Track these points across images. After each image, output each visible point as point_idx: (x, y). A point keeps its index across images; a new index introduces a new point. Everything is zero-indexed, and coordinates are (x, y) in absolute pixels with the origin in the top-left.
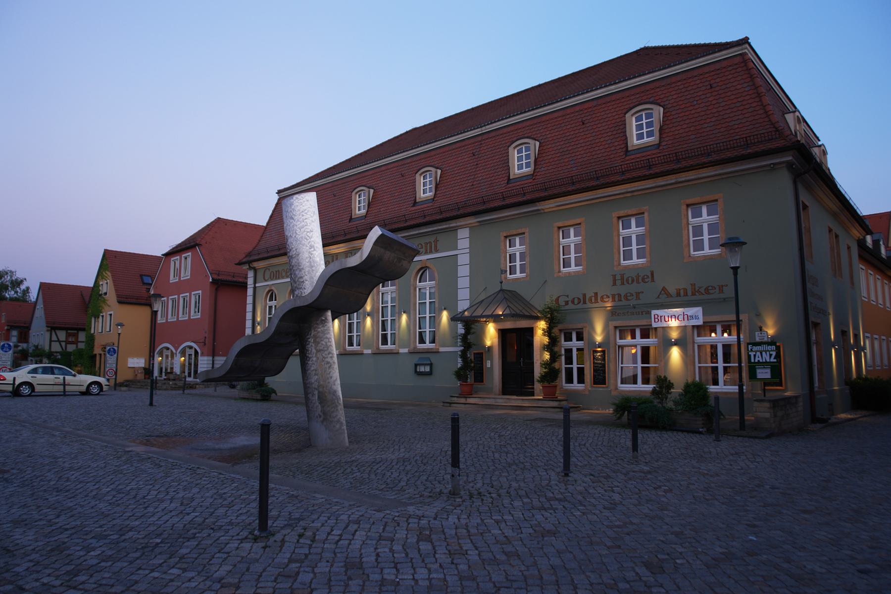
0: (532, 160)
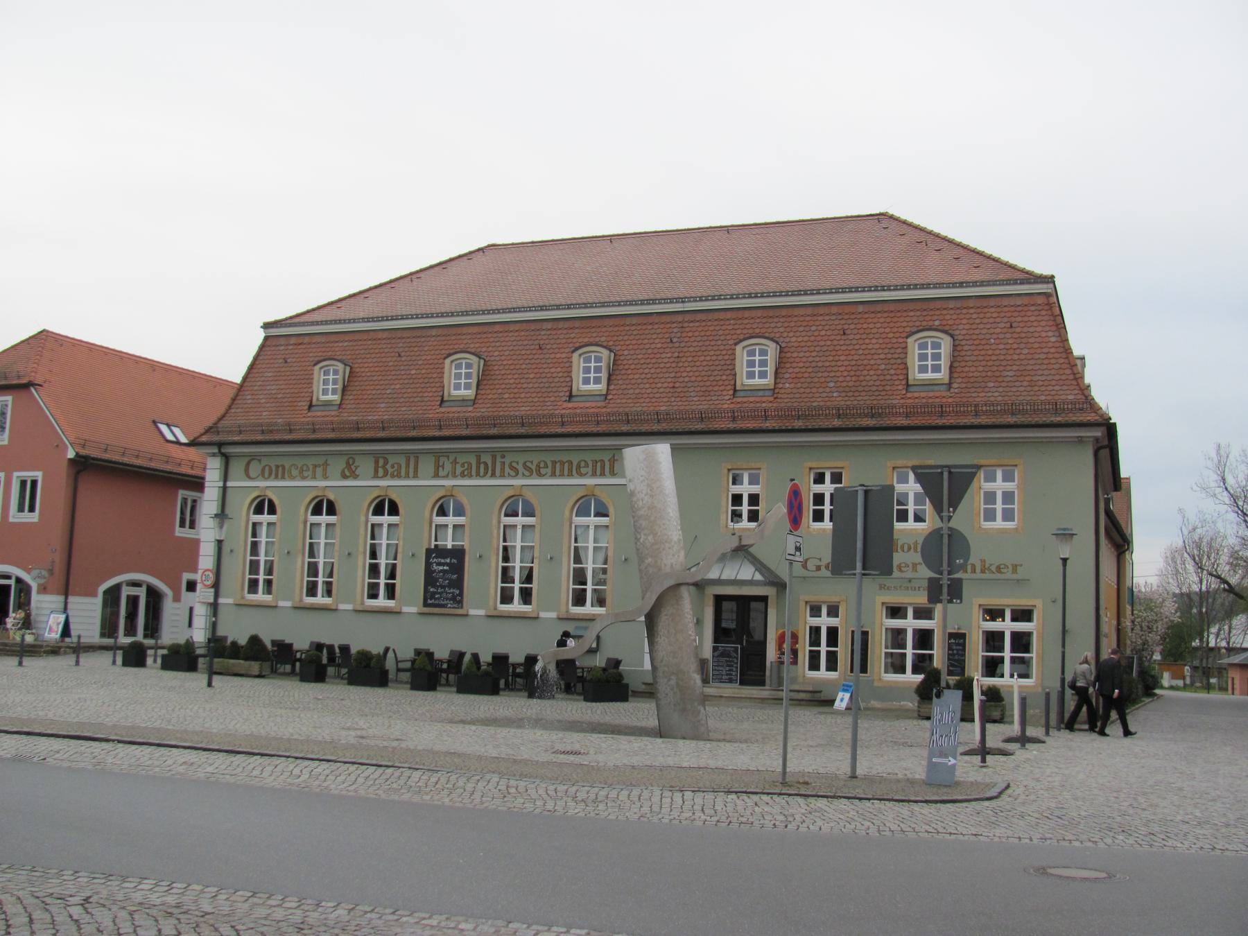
0: (474, 381)
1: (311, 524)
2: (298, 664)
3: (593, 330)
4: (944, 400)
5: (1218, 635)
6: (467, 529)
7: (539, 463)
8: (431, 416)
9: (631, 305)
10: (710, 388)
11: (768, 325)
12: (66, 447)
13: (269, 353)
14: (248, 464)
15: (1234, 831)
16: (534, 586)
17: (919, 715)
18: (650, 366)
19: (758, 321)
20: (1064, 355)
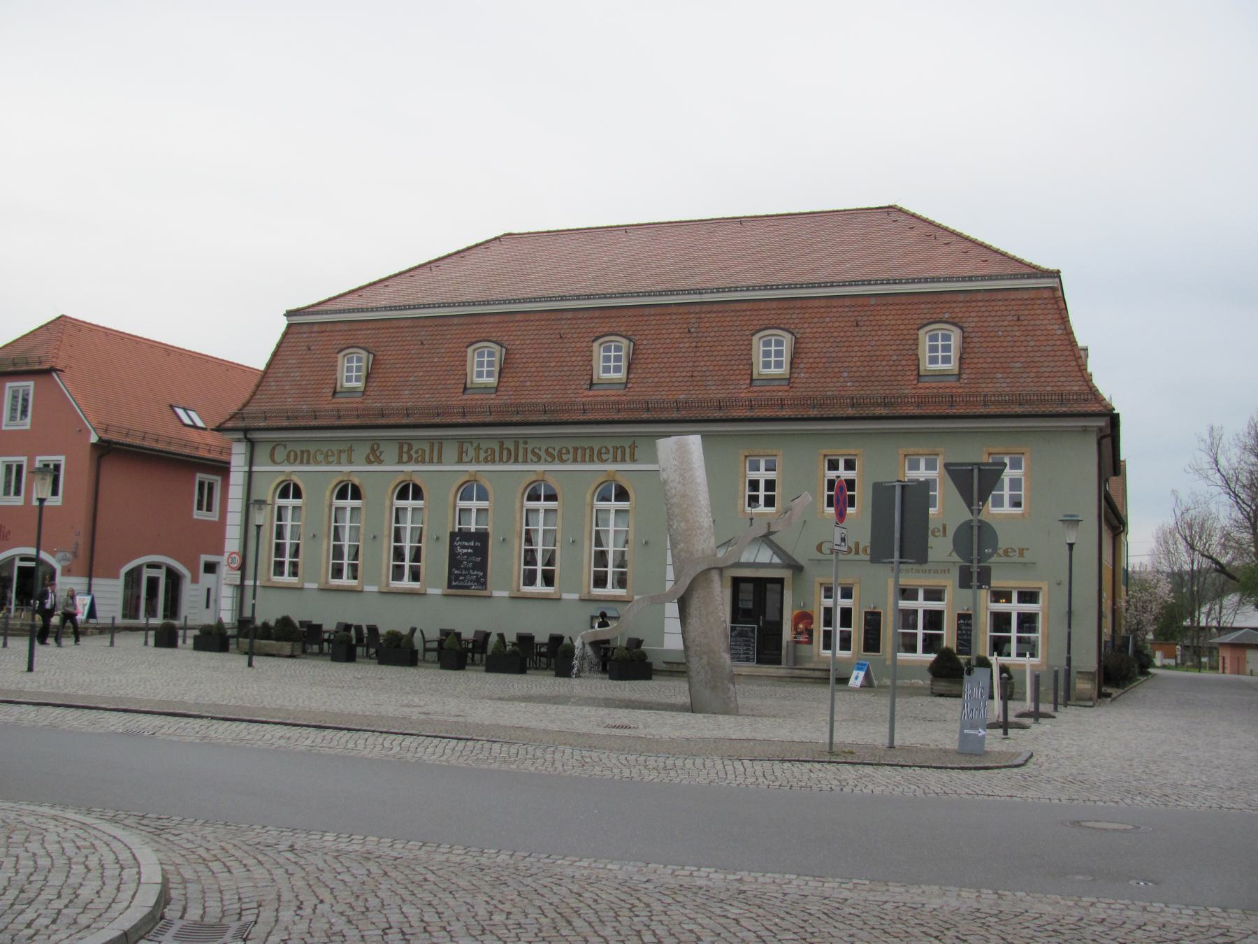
0: (496, 369)
1: (336, 508)
2: (326, 644)
3: (612, 320)
4: (954, 390)
5: (1208, 615)
6: (490, 512)
7: (561, 449)
8: (454, 403)
9: (649, 296)
10: (728, 377)
11: (782, 316)
12: (89, 432)
13: (293, 340)
14: (274, 449)
15: (1238, 793)
16: (557, 568)
17: (932, 693)
18: (669, 355)
19: (773, 312)
20: (1069, 348)
